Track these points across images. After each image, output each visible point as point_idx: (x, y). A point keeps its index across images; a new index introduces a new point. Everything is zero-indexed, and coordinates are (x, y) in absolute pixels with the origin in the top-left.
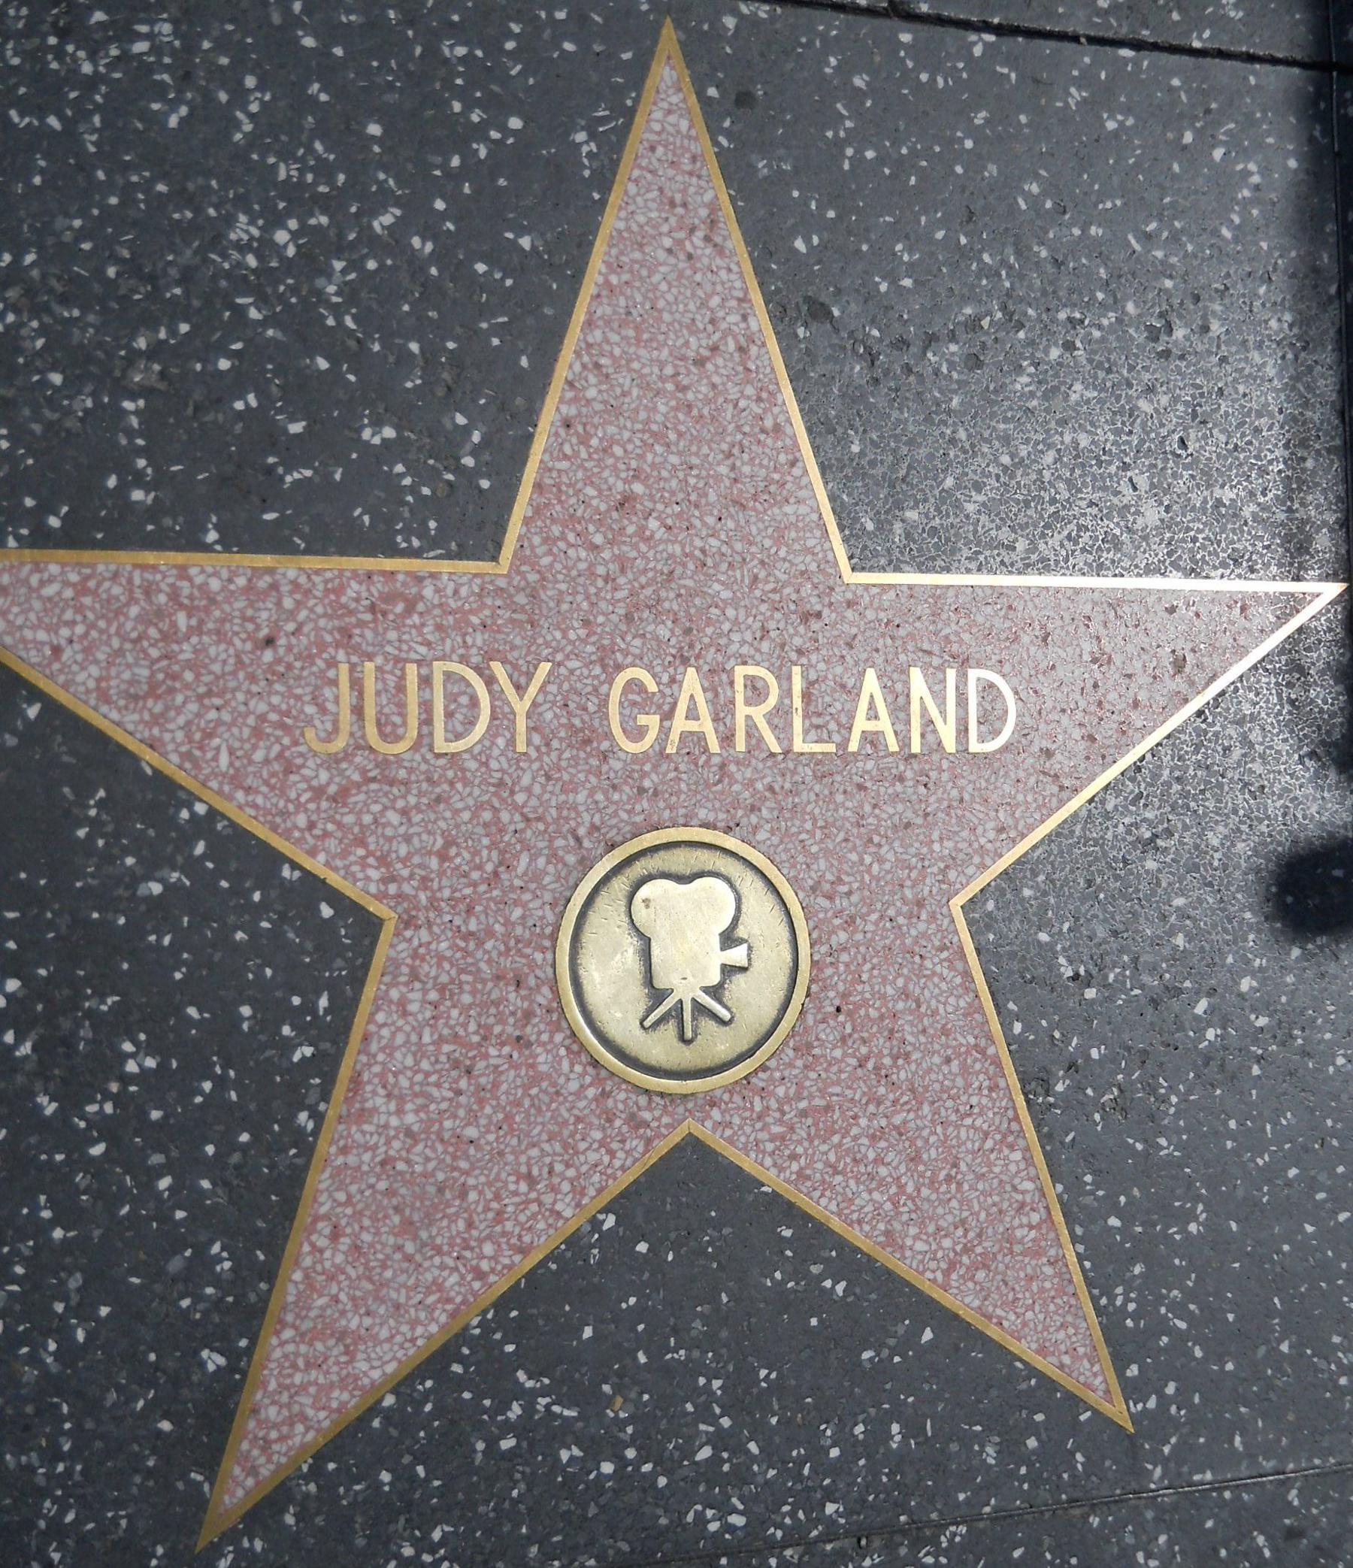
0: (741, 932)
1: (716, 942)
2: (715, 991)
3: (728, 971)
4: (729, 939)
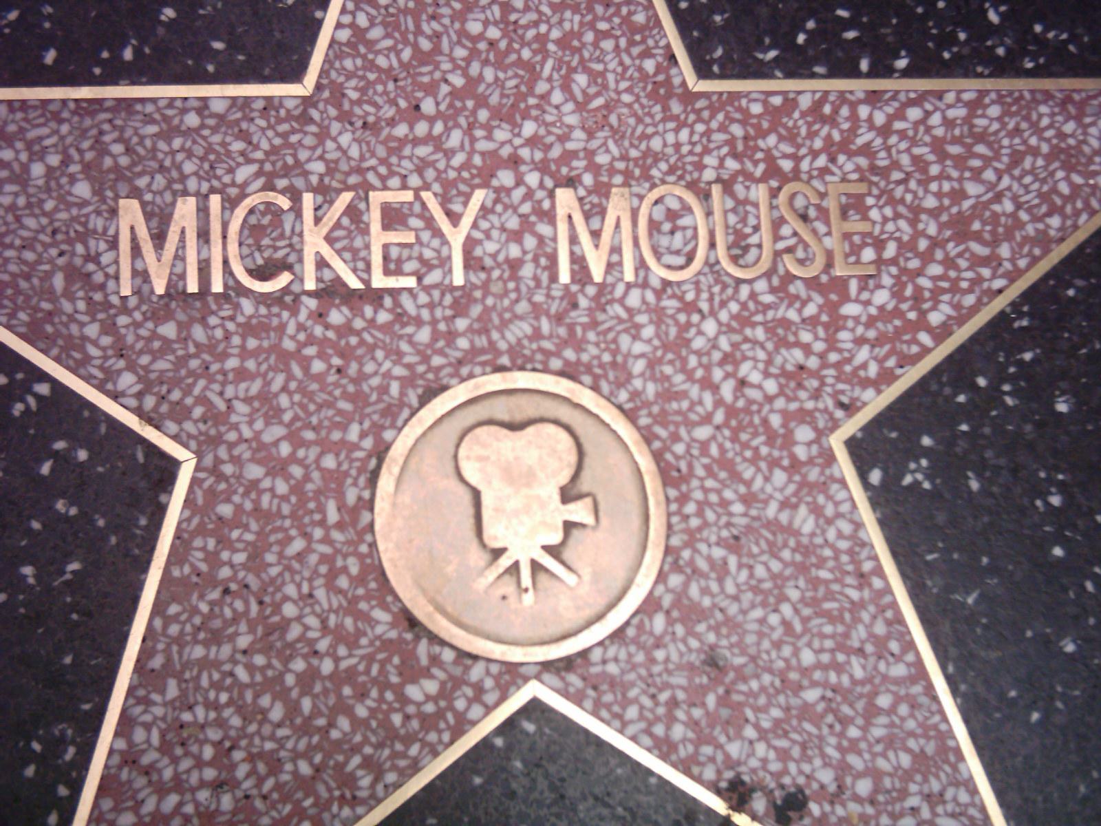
0: (585, 485)
1: (556, 497)
2: (553, 551)
3: (569, 526)
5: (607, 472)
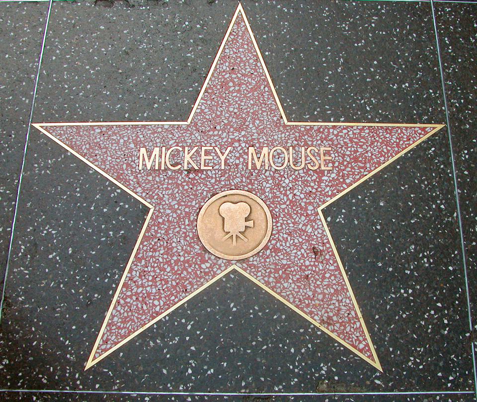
3: (246, 227)
4: (247, 219)
5: (258, 215)
